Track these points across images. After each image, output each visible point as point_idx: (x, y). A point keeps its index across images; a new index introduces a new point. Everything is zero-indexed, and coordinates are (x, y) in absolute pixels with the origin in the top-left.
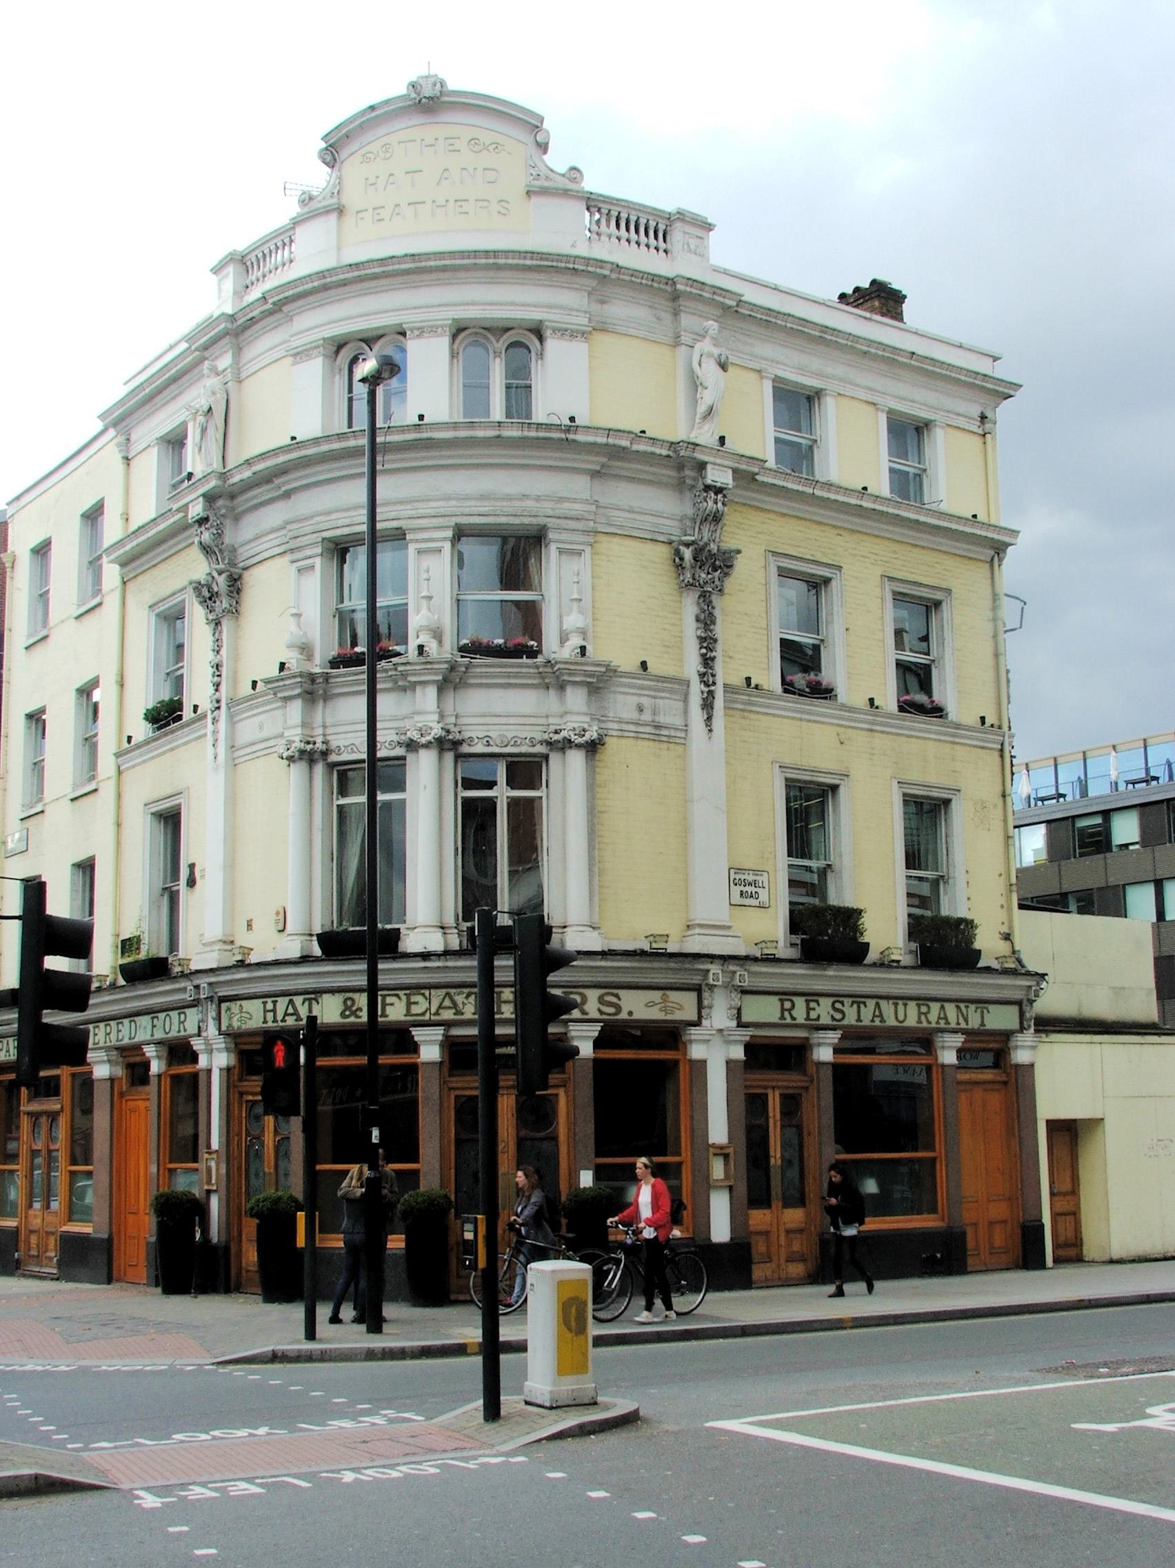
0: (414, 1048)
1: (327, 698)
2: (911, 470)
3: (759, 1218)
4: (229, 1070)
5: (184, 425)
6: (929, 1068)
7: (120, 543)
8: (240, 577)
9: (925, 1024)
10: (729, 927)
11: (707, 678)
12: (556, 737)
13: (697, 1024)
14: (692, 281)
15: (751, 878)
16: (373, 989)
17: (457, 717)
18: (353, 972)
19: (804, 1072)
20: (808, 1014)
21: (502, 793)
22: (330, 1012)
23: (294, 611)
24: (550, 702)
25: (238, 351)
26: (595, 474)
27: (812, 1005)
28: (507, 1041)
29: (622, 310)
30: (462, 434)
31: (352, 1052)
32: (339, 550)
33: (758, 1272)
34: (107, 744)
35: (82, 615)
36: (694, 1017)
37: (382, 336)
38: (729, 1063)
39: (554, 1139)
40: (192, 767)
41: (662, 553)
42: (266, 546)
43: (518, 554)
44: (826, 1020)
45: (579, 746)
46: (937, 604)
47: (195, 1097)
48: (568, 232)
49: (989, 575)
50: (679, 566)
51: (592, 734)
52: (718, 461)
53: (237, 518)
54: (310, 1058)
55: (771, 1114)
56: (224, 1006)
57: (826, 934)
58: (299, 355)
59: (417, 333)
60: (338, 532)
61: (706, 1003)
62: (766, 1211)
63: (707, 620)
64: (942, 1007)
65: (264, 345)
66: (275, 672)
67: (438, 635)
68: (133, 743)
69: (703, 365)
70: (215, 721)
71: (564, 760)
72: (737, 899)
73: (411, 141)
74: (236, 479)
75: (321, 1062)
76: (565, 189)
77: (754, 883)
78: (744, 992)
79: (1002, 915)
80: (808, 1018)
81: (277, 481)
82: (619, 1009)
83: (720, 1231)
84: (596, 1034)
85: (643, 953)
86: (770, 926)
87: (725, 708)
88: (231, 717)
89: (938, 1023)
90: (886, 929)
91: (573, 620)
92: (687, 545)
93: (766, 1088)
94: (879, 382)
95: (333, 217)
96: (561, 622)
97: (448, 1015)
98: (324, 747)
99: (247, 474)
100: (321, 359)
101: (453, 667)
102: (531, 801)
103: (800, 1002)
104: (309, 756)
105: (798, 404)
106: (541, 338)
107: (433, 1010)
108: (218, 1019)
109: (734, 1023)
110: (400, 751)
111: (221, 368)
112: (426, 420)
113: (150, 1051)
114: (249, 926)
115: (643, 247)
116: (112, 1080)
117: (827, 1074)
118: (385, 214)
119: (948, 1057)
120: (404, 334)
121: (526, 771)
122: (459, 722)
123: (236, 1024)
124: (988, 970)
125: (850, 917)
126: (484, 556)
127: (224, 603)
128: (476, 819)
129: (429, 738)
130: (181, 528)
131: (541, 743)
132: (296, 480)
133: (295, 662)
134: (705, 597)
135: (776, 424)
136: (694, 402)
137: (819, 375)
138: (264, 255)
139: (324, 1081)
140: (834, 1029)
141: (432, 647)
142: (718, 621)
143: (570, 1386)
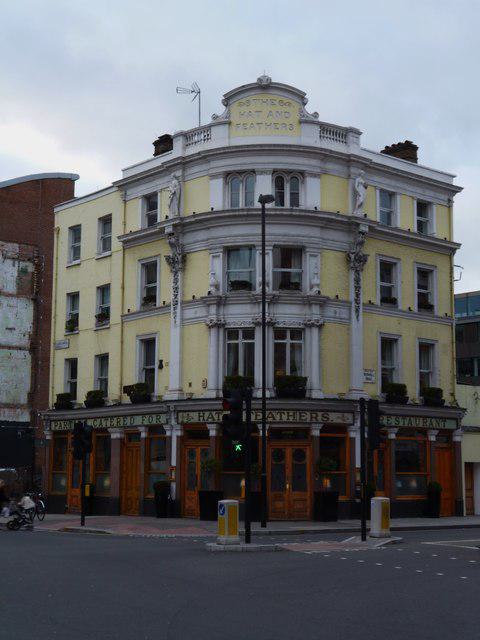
1: (224, 305)
6: (425, 442)
11: (357, 301)
14: (356, 156)
24: (306, 310)
29: (330, 166)
38: (178, 437)
43: (289, 255)
48: (311, 138)
50: (348, 260)
56: (180, 414)
57: (394, 392)
58: (213, 177)
63: (357, 281)
73: (256, 102)
79: (450, 387)
86: (374, 391)
95: (227, 126)
104: (218, 326)
105: (388, 197)
113: (141, 429)
114: (190, 385)
116: (121, 439)
128: (279, 349)
134: (357, 272)
137: (394, 187)
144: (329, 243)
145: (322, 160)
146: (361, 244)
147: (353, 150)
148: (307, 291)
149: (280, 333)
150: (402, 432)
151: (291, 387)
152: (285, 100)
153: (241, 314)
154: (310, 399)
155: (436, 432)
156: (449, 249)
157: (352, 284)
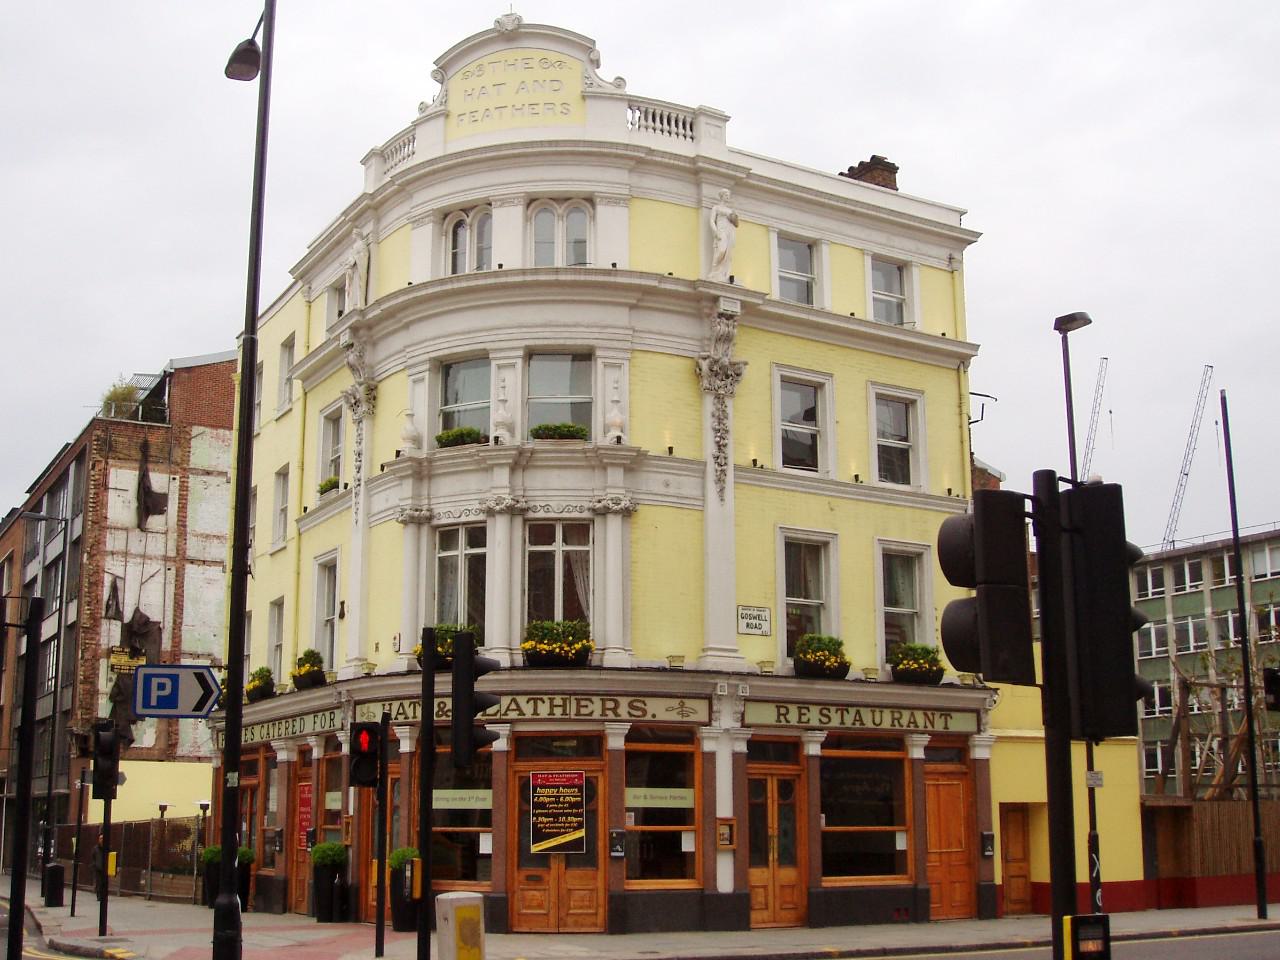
1: (431, 477)
2: (894, 300)
3: (758, 875)
8: (376, 387)
9: (897, 727)
10: (735, 651)
11: (720, 460)
12: (598, 505)
13: (709, 724)
15: (755, 613)
17: (524, 490)
20: (800, 718)
21: (559, 547)
23: (409, 412)
25: (378, 220)
27: (804, 711)
29: (651, 182)
30: (529, 278)
33: (755, 916)
34: (294, 513)
35: (279, 418)
36: (706, 720)
37: (476, 206)
41: (682, 366)
42: (391, 365)
44: (814, 722)
45: (501, 512)
46: (914, 402)
48: (620, 128)
49: (956, 378)
50: (699, 375)
52: (729, 295)
53: (374, 344)
55: (769, 795)
56: (358, 707)
57: (813, 657)
58: (417, 222)
59: (499, 203)
60: (441, 353)
61: (715, 708)
62: (765, 869)
63: (721, 418)
64: (912, 714)
65: (396, 214)
67: (511, 429)
68: (308, 511)
69: (718, 223)
71: (605, 523)
73: (498, 65)
74: (370, 316)
76: (617, 95)
77: (758, 617)
80: (800, 721)
81: (400, 316)
82: (645, 712)
83: (725, 883)
84: (823, 739)
85: (664, 670)
86: (767, 650)
87: (735, 482)
88: (368, 491)
89: (909, 726)
92: (705, 359)
93: (765, 774)
94: (863, 233)
95: (442, 119)
96: (604, 417)
97: (513, 715)
98: (428, 514)
99: (377, 312)
100: (430, 226)
104: (417, 520)
106: (593, 205)
107: (503, 712)
109: (739, 725)
111: (365, 234)
112: (504, 268)
113: (312, 741)
115: (658, 132)
116: (289, 763)
117: (815, 767)
118: (478, 116)
119: (918, 753)
120: (490, 204)
121: (578, 531)
122: (527, 494)
125: (835, 646)
127: (364, 407)
128: (539, 572)
129: (502, 506)
131: (589, 509)
132: (413, 314)
133: (407, 449)
138: (396, 149)
140: (821, 730)
142: (730, 416)
145: (631, 171)
146: (727, 339)
147: (705, 147)
148: (601, 438)
149: (541, 532)
150: (834, 740)
151: (560, 641)
153: (459, 495)
154: (600, 668)
155: (925, 739)
156: (957, 358)
157: (709, 423)
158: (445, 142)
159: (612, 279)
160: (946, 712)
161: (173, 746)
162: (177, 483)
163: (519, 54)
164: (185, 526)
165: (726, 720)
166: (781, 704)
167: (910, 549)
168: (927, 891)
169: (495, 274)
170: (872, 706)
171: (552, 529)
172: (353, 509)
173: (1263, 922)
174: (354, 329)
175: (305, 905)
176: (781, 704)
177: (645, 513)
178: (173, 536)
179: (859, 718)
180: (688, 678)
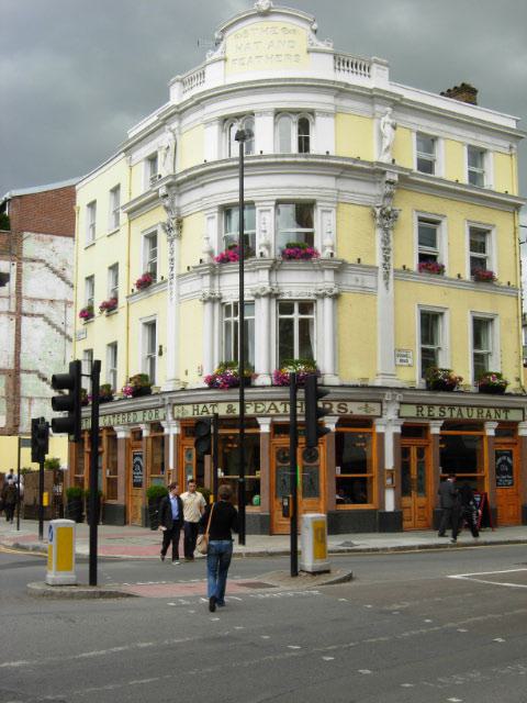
0: (258, 426)
1: (220, 275)
3: (407, 501)
4: (177, 436)
5: (156, 152)
7: (128, 204)
13: (380, 417)
16: (242, 402)
18: (235, 394)
19: (427, 438)
21: (296, 316)
22: (222, 410)
25: (181, 120)
26: (337, 177)
28: (301, 424)
29: (347, 103)
30: (279, 160)
31: (233, 427)
32: (226, 210)
33: (405, 524)
39: (318, 466)
40: (157, 305)
42: (193, 208)
43: (304, 212)
44: (437, 415)
47: (163, 445)
50: (374, 216)
51: (335, 291)
53: (180, 195)
54: (216, 430)
56: (176, 408)
57: (440, 383)
58: (208, 123)
65: (192, 118)
66: (197, 263)
67: (268, 247)
70: (171, 283)
72: (398, 363)
74: (179, 179)
75: (220, 431)
78: (401, 403)
82: (347, 411)
83: (390, 506)
85: (357, 386)
86: (412, 375)
90: (464, 372)
91: (328, 241)
95: (223, 62)
97: (272, 412)
101: (275, 261)
102: (307, 320)
103: (425, 408)
104: (213, 300)
105: (427, 142)
108: (173, 413)
110: (252, 298)
113: (143, 426)
114: (187, 373)
116: (126, 439)
118: (246, 61)
119: (490, 432)
121: (306, 307)
123: (180, 415)
124: (510, 395)
126: (290, 210)
127: (174, 233)
128: (285, 328)
130: (156, 198)
135: (418, 150)
136: (381, 143)
139: (221, 443)
141: (266, 253)
143: (320, 564)
144: (348, 196)
145: (336, 96)
149: (285, 307)
150: (448, 425)
152: (290, 27)
155: (495, 425)
158: (225, 76)
159: (327, 161)
160: (507, 409)
161: (17, 426)
162: (15, 267)
163: (270, 25)
164: (20, 293)
165: (391, 414)
166: (419, 405)
167: (487, 316)
168: (496, 509)
169: (259, 157)
170: (468, 406)
171: (293, 306)
172: (169, 292)
173: (92, 589)
174: (169, 186)
175: (139, 521)
176: (419, 405)
177: (347, 298)
178: (14, 299)
179: (460, 412)
180: (370, 391)
